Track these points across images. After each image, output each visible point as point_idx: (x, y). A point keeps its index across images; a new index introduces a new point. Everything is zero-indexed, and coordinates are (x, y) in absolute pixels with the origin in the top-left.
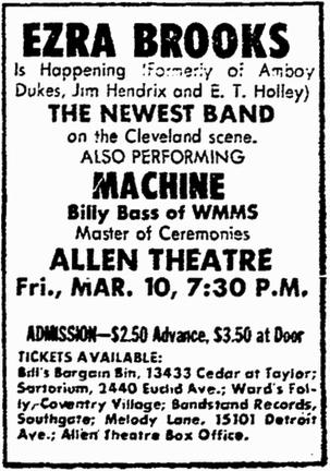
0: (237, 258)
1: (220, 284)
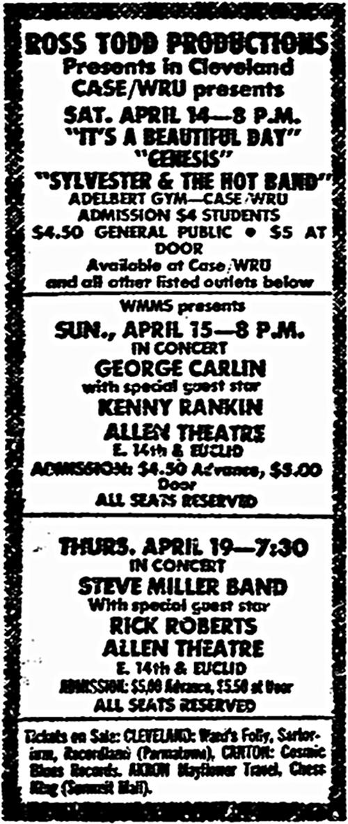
0: (239, 433)
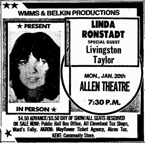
1: (97, 101)
